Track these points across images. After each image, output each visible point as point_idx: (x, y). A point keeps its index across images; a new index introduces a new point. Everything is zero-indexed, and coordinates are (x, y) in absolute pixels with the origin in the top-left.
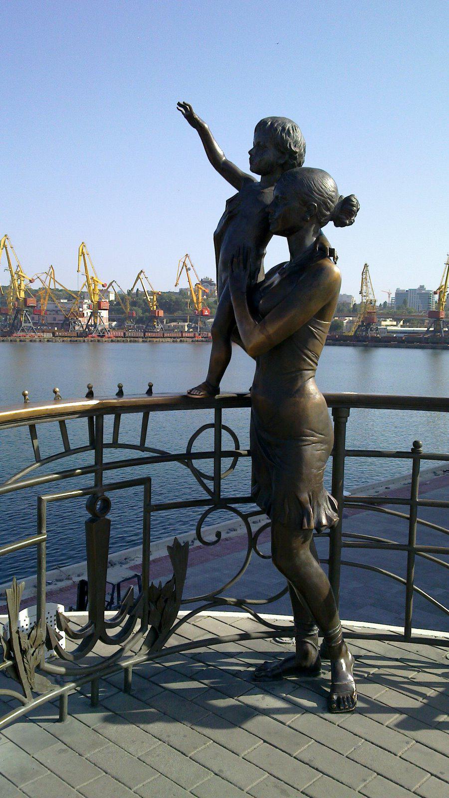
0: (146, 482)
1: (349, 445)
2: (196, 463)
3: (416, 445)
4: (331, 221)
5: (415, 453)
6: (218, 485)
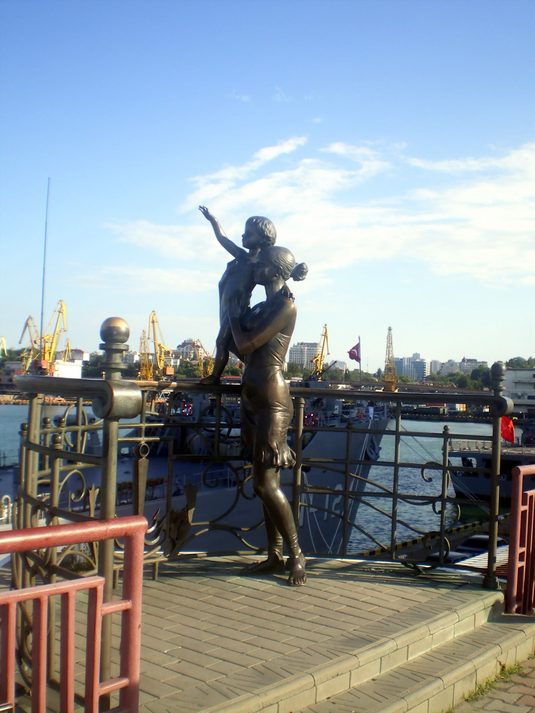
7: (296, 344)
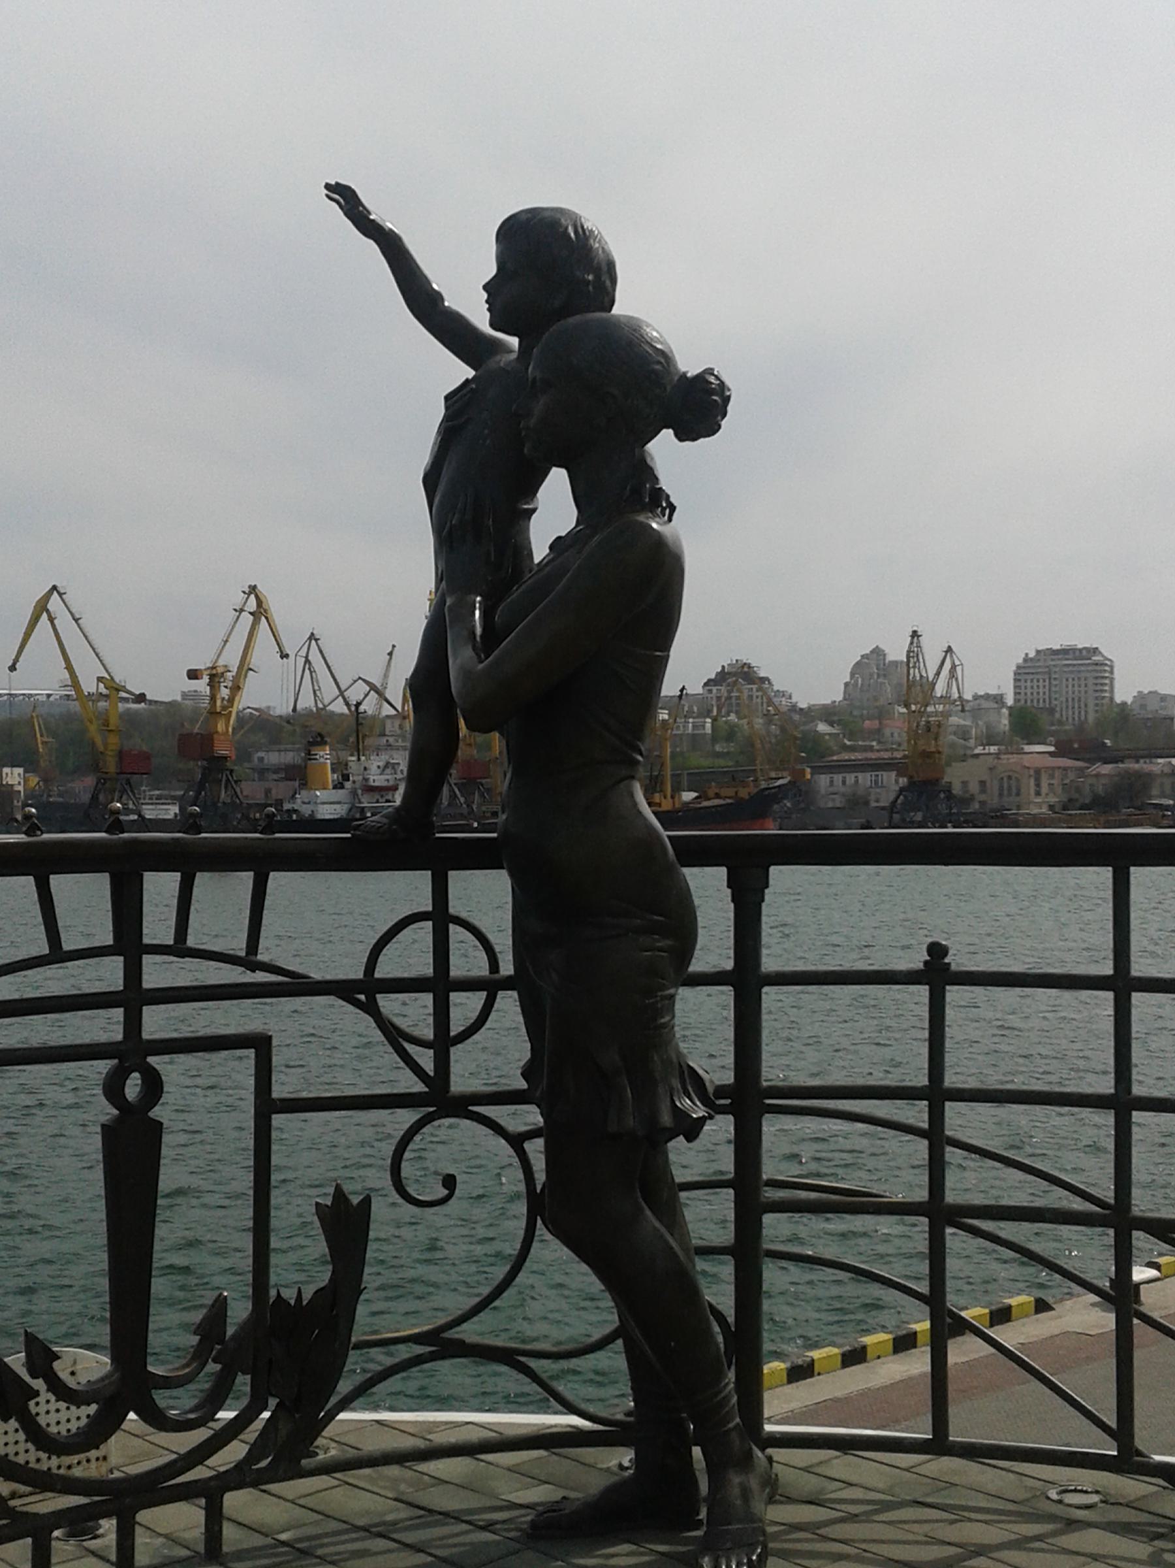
0: (261, 1044)
1: (770, 963)
2: (388, 1003)
3: (937, 951)
4: (668, 427)
5: (937, 973)
6: (443, 1063)
7: (1032, 655)
